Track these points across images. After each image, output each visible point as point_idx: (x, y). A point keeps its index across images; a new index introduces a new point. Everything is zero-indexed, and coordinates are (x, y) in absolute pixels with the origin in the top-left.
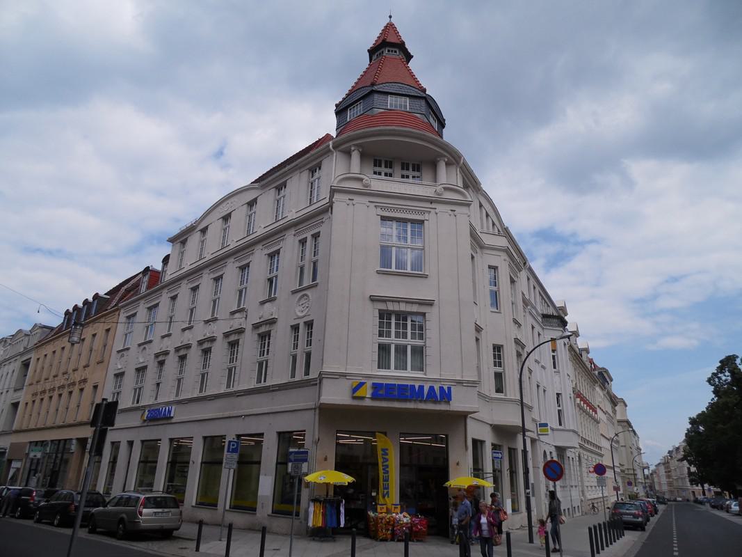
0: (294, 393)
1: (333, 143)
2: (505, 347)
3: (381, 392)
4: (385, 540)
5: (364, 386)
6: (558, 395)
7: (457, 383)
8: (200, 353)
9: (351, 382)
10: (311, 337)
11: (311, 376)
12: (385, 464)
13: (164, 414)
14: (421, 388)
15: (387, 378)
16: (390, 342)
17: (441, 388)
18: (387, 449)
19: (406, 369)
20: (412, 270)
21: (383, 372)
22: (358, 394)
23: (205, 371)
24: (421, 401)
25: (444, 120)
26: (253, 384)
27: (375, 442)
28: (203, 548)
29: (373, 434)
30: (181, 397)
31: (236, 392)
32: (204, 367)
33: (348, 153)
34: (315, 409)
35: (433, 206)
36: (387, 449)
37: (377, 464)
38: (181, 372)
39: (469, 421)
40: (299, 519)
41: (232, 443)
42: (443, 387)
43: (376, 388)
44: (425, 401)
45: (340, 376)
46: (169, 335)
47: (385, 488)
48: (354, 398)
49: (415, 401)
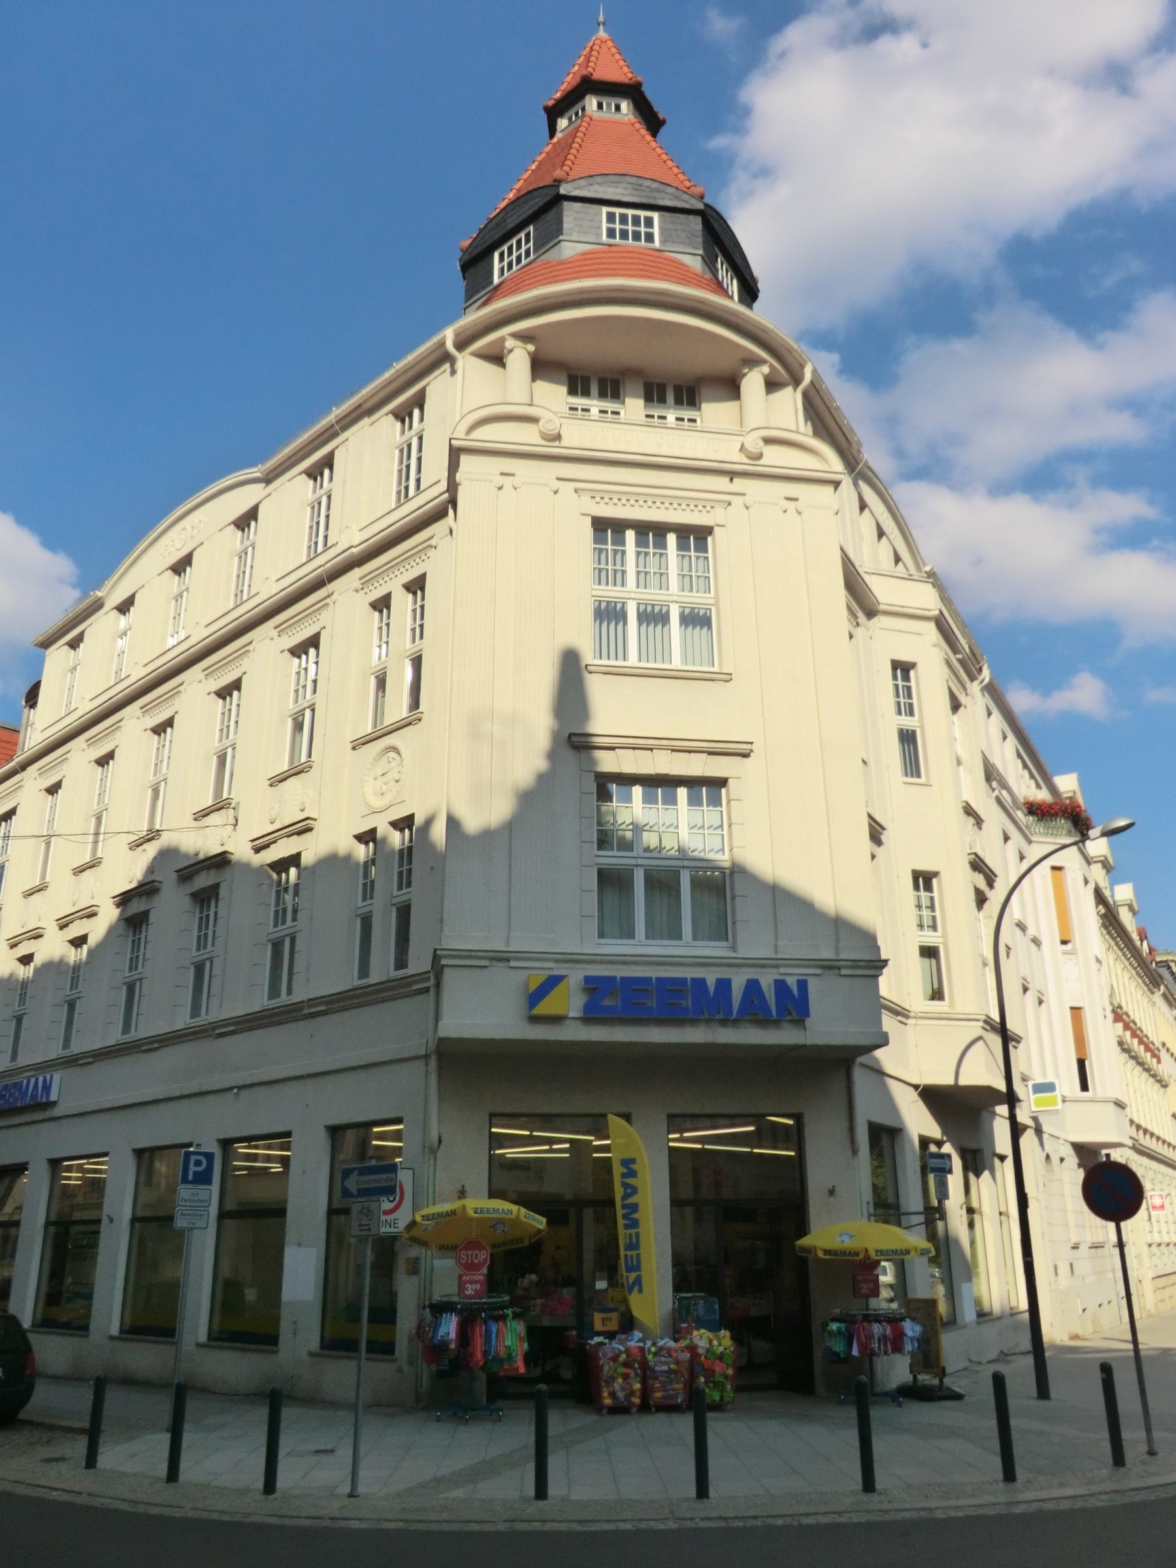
0: (366, 1017)
1: (457, 335)
2: (944, 875)
3: (607, 1002)
4: (620, 1409)
5: (563, 984)
6: (1076, 1011)
7: (823, 967)
8: (187, 902)
9: (522, 976)
10: (410, 862)
11: (411, 970)
12: (627, 1202)
13: (34, 1096)
14: (724, 985)
15: (635, 963)
16: (633, 862)
17: (780, 986)
18: (633, 1161)
19: (680, 938)
20: (685, 661)
21: (615, 947)
22: (545, 1007)
23: (204, 954)
24: (724, 1023)
25: (755, 281)
26: (260, 1001)
27: (606, 1149)
28: (108, 1458)
29: (598, 1125)
30: (77, 1047)
31: (214, 1026)
32: (202, 942)
33: (497, 358)
34: (426, 1057)
35: (739, 484)
36: (633, 1161)
37: (611, 1203)
38: (133, 964)
39: (858, 1075)
40: (395, 1360)
41: (193, 1158)
42: (783, 982)
43: (595, 989)
44: (736, 1023)
45: (492, 959)
46: (41, 889)
47: (630, 1269)
48: (535, 1020)
49: (708, 1021)
